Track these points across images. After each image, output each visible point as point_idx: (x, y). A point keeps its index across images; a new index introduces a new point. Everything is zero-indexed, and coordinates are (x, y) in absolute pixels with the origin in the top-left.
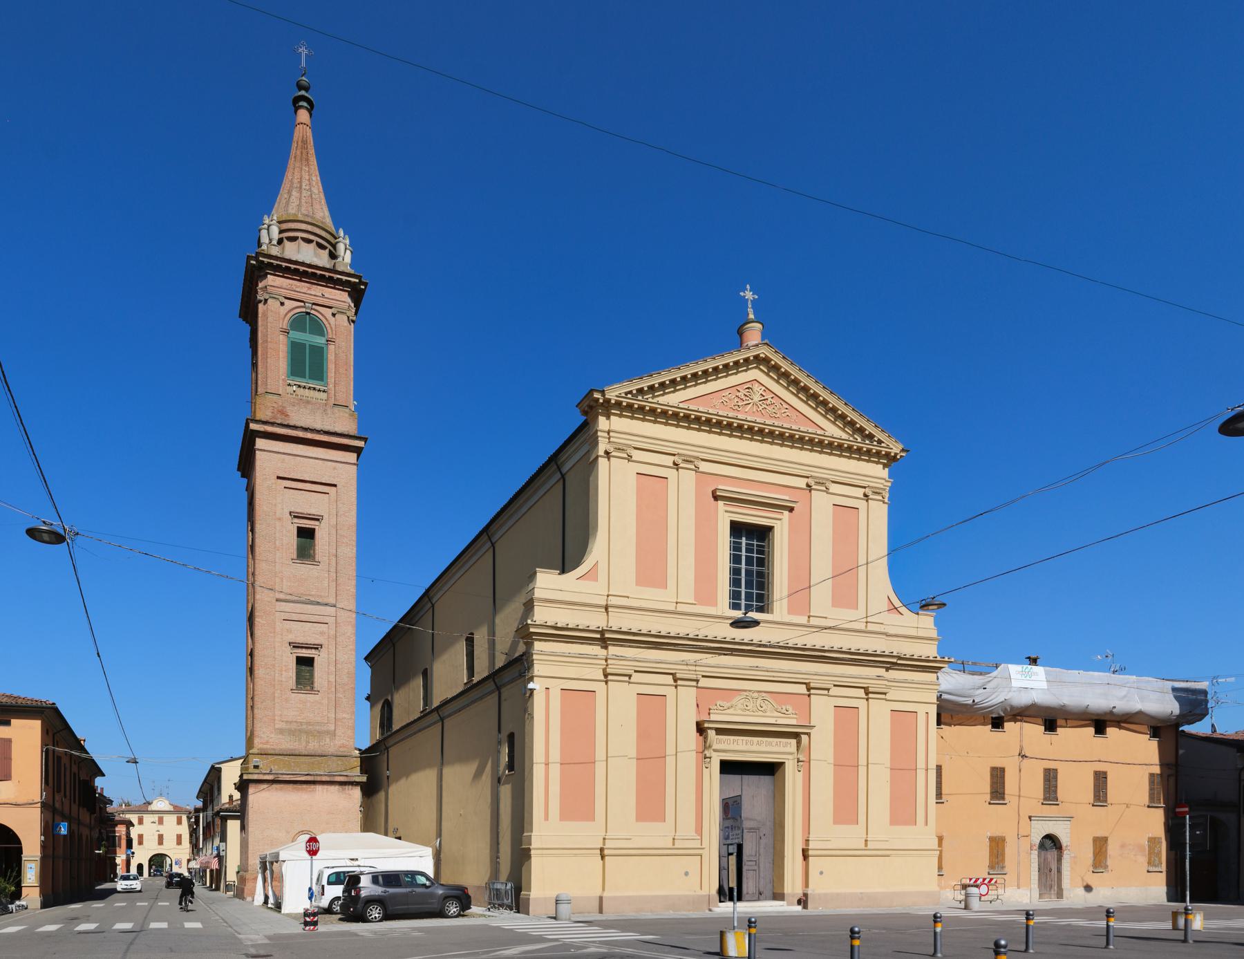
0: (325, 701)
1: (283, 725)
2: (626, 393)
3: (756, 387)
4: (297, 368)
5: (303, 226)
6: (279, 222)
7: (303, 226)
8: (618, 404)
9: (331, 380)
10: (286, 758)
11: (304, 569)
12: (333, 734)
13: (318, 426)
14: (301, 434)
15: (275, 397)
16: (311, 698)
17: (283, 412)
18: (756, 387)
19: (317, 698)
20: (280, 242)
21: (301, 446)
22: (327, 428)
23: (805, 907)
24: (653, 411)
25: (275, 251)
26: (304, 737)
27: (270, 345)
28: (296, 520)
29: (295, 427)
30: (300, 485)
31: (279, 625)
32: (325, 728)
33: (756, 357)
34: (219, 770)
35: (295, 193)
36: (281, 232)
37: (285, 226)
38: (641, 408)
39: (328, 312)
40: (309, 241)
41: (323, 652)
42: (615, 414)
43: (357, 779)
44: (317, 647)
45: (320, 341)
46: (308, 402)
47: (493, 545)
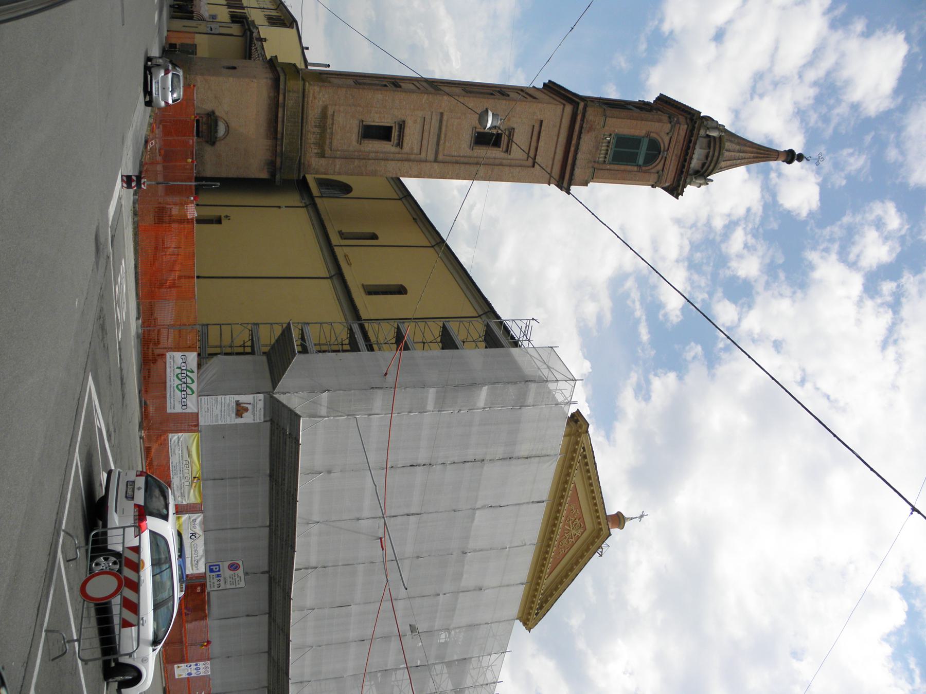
0: (351, 148)
1: (330, 112)
2: (584, 448)
3: (580, 531)
4: (622, 141)
5: (716, 154)
6: (720, 137)
7: (716, 154)
8: (577, 443)
9: (612, 167)
10: (30, 640)
11: (467, 137)
12: (322, 155)
13: (579, 156)
14: (574, 142)
15: (602, 124)
16: (354, 137)
17: (591, 129)
18: (580, 531)
19: (354, 143)
20: (708, 136)
21: (565, 141)
22: (578, 162)
23: (238, 404)
24: (570, 467)
25: (702, 132)
26: (317, 130)
27: (639, 122)
28: (507, 133)
29: (579, 138)
30: (535, 138)
31: (420, 114)
32: (327, 148)
33: (601, 529)
34: (291, 26)
35: (738, 147)
36: (714, 137)
37: (717, 140)
38: (573, 459)
39: (660, 167)
40: (707, 157)
41: (394, 149)
42: (570, 440)
43: (278, 177)
44: (400, 144)
45: (641, 161)
46: (597, 148)
47: (480, 316)
